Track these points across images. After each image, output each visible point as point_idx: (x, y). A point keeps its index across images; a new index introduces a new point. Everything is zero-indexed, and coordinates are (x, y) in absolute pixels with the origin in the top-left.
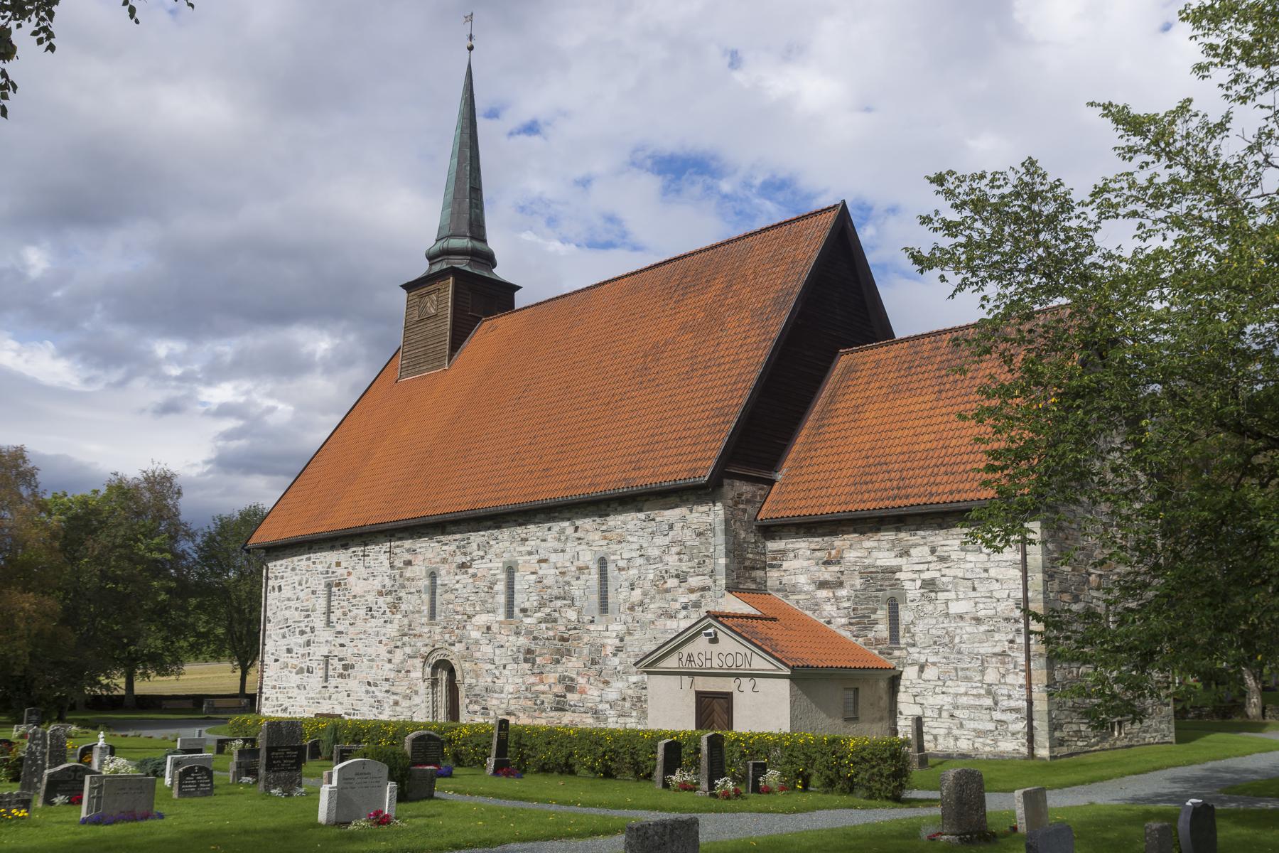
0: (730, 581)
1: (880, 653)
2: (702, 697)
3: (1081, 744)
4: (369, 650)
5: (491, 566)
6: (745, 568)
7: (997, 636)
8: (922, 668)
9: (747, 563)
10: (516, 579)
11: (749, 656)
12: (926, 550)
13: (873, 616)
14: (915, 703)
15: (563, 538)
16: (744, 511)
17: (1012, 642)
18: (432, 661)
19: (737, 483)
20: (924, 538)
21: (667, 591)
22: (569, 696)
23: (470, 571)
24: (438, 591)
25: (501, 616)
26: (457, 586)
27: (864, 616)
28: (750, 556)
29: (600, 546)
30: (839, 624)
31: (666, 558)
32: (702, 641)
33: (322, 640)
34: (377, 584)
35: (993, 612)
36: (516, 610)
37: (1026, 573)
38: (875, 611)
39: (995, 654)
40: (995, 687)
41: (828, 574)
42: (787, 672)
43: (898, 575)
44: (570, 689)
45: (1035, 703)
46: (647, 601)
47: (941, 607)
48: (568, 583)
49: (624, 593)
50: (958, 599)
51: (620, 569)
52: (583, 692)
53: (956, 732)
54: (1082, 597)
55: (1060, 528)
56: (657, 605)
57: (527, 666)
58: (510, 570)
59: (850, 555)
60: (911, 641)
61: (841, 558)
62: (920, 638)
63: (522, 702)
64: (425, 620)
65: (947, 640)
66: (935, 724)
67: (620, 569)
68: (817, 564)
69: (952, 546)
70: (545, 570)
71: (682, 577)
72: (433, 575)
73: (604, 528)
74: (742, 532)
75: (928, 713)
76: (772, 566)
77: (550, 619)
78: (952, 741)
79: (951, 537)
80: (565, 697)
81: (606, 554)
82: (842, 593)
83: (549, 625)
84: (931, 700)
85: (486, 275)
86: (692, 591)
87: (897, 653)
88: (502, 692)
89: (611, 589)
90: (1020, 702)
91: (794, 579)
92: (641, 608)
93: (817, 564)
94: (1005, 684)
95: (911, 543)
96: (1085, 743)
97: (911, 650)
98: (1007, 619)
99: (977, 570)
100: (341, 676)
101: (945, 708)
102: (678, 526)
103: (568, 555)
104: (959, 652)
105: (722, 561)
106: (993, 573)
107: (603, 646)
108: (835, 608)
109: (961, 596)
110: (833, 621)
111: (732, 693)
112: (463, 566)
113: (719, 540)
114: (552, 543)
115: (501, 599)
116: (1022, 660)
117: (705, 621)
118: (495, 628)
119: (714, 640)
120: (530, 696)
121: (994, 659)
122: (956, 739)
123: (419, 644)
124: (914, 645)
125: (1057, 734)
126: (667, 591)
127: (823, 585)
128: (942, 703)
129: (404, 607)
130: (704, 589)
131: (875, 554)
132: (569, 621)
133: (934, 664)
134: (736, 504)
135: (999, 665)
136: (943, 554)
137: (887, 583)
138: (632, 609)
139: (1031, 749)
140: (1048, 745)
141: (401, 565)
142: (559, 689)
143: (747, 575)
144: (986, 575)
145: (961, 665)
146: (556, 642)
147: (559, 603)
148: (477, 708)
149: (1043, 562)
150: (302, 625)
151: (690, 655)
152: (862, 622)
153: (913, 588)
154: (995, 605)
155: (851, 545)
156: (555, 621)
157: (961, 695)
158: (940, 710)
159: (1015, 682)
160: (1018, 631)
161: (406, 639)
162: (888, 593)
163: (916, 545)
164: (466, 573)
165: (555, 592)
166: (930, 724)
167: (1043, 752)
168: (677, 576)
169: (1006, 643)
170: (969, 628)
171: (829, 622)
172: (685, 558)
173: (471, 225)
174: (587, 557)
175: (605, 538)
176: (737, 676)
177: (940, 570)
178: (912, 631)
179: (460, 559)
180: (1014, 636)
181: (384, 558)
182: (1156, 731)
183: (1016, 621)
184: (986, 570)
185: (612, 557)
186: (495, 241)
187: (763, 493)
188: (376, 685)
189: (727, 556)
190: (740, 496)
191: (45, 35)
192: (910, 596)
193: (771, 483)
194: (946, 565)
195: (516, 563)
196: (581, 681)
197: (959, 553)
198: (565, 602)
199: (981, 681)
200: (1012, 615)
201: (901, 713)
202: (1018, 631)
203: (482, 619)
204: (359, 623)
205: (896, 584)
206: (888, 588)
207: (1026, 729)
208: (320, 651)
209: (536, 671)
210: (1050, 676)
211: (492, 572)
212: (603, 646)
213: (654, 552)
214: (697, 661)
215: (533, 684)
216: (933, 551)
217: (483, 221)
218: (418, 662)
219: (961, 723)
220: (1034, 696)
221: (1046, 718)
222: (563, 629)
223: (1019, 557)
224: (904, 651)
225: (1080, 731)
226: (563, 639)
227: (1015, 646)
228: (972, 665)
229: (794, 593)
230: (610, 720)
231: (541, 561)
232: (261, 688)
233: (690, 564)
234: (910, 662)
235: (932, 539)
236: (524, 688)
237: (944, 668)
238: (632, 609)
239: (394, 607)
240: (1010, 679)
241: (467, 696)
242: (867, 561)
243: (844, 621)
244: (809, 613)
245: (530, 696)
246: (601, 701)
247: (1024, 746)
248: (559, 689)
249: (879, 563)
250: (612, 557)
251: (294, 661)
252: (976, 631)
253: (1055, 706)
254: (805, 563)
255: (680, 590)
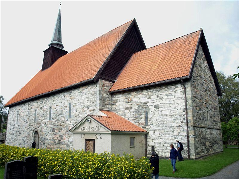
0: (100, 108)
1: (142, 127)
2: (86, 140)
3: (203, 153)
4: (24, 129)
5: (46, 108)
6: (105, 104)
7: (177, 121)
8: (155, 131)
9: (106, 103)
10: (52, 110)
11: (100, 127)
12: (156, 96)
13: (140, 117)
14: (153, 142)
15: (62, 99)
16: (105, 89)
17: (182, 122)
18: (34, 132)
19: (103, 81)
20: (155, 93)
21: (85, 111)
22: (61, 140)
23: (43, 109)
24: (37, 114)
25: (48, 120)
26: (40, 113)
27: (138, 117)
28: (107, 101)
29: (69, 101)
30: (131, 120)
31: (84, 102)
32: (87, 123)
33: (16, 127)
34: (25, 114)
35: (176, 113)
36: (51, 118)
37: (186, 101)
38: (141, 115)
39: (177, 126)
40: (177, 137)
41: (128, 105)
42: (110, 132)
43: (147, 104)
44: (62, 139)
45: (190, 141)
46: (80, 114)
47: (160, 113)
48: (62, 111)
49: (75, 112)
50: (165, 110)
51: (74, 106)
52: (64, 139)
53: (165, 151)
54: (201, 109)
55: (195, 88)
56: (82, 115)
57: (53, 132)
58: (50, 108)
59: (134, 100)
60: (151, 123)
61: (132, 100)
62: (154, 123)
63: (52, 142)
64: (33, 122)
65: (162, 123)
66: (158, 148)
67: (74, 106)
68: (125, 103)
69: (163, 94)
70: (58, 108)
71: (88, 107)
72: (36, 110)
73: (71, 96)
74: (104, 94)
75: (156, 145)
76: (113, 104)
77: (58, 120)
78: (164, 153)
79: (163, 92)
80: (60, 141)
81: (71, 102)
82: (131, 110)
83: (58, 122)
84: (158, 141)
85: (62, 49)
86: (90, 111)
87: (147, 127)
88: (47, 139)
89: (71, 111)
90: (185, 141)
91: (119, 108)
92: (78, 117)
93: (125, 103)
94: (180, 135)
95: (151, 95)
96: (204, 153)
97: (151, 126)
98: (180, 115)
99: (171, 101)
100: (19, 135)
101: (161, 143)
102: (87, 93)
103: (62, 104)
104: (166, 126)
105: (98, 102)
106: (176, 101)
107: (69, 127)
108: (130, 115)
109: (166, 109)
110: (129, 118)
111: (95, 139)
112: (41, 108)
113: (98, 96)
114: (59, 101)
115: (48, 116)
116: (185, 128)
117: (87, 117)
118: (47, 123)
119: (90, 122)
120: (53, 140)
121: (177, 128)
122: (165, 153)
123: (32, 128)
124: (152, 125)
125: (197, 151)
126: (85, 111)
127: (127, 108)
128: (160, 142)
129: (30, 119)
130: (93, 110)
131: (141, 99)
132: (62, 120)
133: (158, 130)
134: (103, 86)
135: (178, 130)
136: (160, 97)
137: (144, 107)
138: (76, 117)
139: (189, 156)
140: (194, 155)
141: (30, 109)
142: (59, 139)
143: (106, 106)
144: (174, 102)
145: (166, 130)
146: (59, 126)
147: (60, 116)
148: (42, 143)
149: (191, 97)
150: (13, 124)
151: (84, 128)
152: (137, 118)
153: (152, 108)
154: (177, 111)
155: (134, 97)
156: (59, 121)
157: (166, 139)
158: (160, 144)
159: (183, 135)
160: (184, 119)
161: (30, 126)
162: (145, 110)
163: (152, 95)
164: (42, 110)
165: (59, 113)
166: (157, 148)
167: (193, 157)
168: (87, 107)
169: (180, 123)
170: (169, 119)
171: (128, 119)
172: (89, 102)
173: (58, 39)
174: (67, 104)
175: (71, 98)
176: (96, 134)
177: (160, 102)
178: (152, 120)
179: (41, 106)
180: (183, 120)
181: (27, 107)
182: (219, 148)
183: (183, 116)
184: (174, 101)
185: (72, 103)
186: (63, 43)
187: (111, 84)
188: (24, 138)
189: (99, 100)
190: (104, 84)
191: (172, 146)
192: (151, 110)
193: (114, 82)
194: (161, 100)
195: (52, 106)
196: (64, 136)
197: (166, 96)
198: (61, 116)
199: (173, 135)
200: (182, 114)
201: (148, 145)
202: (184, 119)
203: (44, 121)
204: (22, 123)
205: (147, 107)
206: (145, 108)
207: (187, 149)
208: (16, 130)
209: (55, 134)
210: (195, 132)
211: (47, 109)
212: (69, 127)
213: (81, 101)
214: (86, 129)
215: (54, 137)
216: (158, 96)
217: (61, 38)
218: (32, 132)
219: (166, 148)
220: (190, 139)
221: (194, 146)
222: (61, 123)
223: (184, 96)
224: (149, 126)
225: (203, 150)
226: (61, 126)
227: (183, 123)
228: (170, 130)
229: (119, 111)
230: (70, 147)
231: (57, 105)
232: (5, 138)
233: (90, 103)
234: (151, 130)
235: (157, 93)
236: (52, 138)
237: (161, 131)
238: (76, 117)
239: (28, 119)
240: (182, 134)
241: (41, 140)
242: (139, 101)
243: (133, 118)
244: (123, 117)
245: (53, 140)
246: (68, 142)
247: (186, 155)
248: (59, 139)
249: (142, 101)
250: (72, 103)
251: (11, 132)
252: (171, 119)
253: (196, 142)
254: (122, 103)
255: (88, 111)
